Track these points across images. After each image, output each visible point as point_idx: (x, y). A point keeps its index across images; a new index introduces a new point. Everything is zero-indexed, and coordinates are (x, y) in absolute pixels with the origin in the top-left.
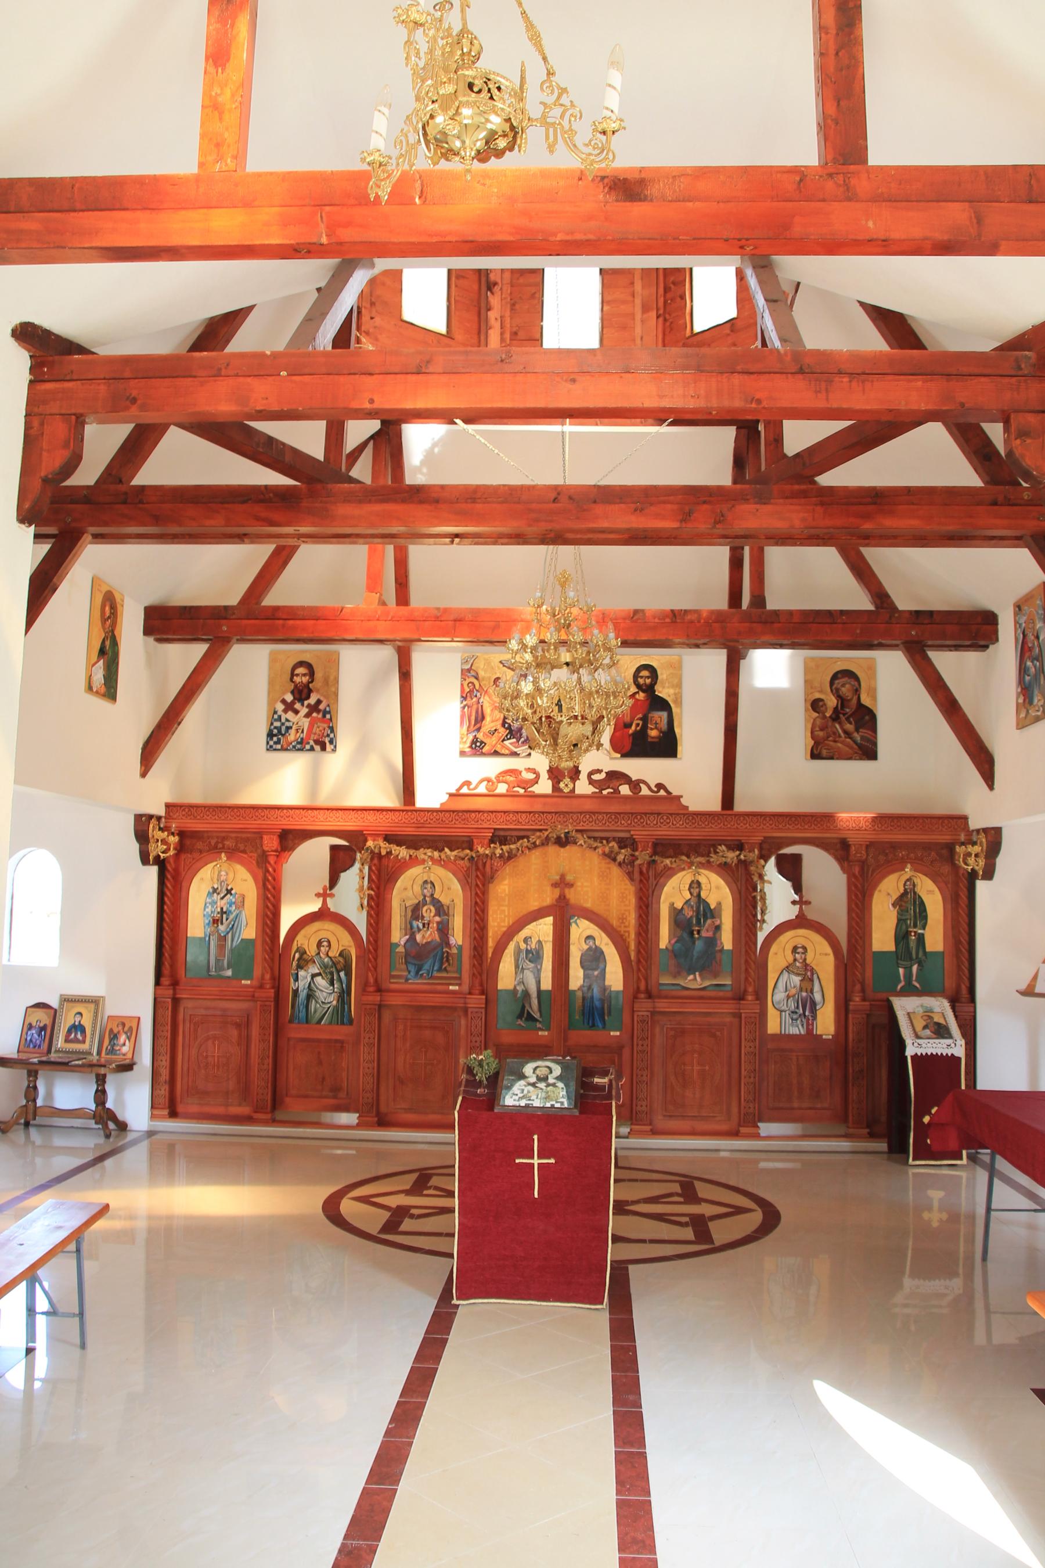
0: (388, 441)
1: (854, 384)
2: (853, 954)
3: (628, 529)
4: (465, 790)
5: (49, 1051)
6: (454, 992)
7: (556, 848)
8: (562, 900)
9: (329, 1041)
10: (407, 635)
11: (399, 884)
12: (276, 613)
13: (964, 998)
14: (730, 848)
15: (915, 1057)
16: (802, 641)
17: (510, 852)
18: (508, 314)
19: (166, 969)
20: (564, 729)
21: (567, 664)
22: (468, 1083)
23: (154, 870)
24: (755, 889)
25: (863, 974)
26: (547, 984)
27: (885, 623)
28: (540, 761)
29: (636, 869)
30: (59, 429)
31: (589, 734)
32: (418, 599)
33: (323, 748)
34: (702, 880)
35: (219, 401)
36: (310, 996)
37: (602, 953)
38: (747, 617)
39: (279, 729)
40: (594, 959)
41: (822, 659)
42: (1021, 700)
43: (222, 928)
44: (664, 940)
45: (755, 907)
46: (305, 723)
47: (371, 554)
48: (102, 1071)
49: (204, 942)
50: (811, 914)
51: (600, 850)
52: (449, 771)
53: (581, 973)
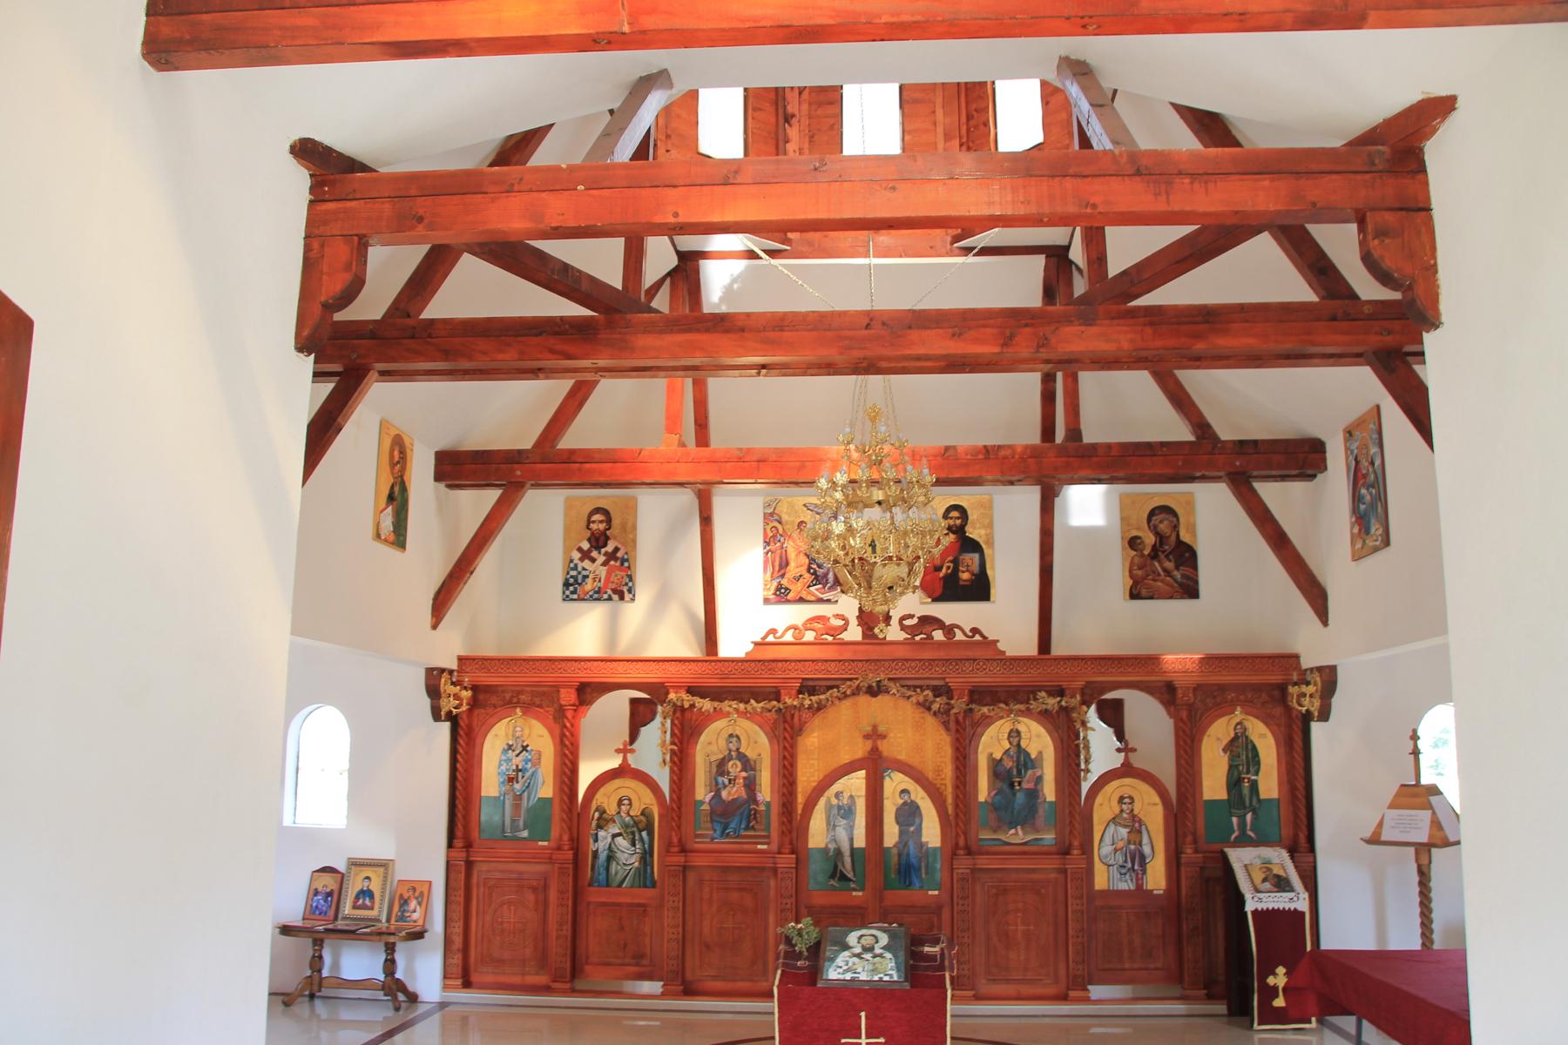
0: (687, 269)
1: (1196, 185)
2: (1181, 802)
3: (945, 357)
4: (771, 639)
5: (336, 918)
6: (762, 852)
7: (868, 698)
8: (875, 751)
9: (631, 905)
10: (708, 478)
11: (703, 738)
12: (571, 456)
13: (1302, 845)
14: (1051, 694)
15: (1255, 912)
16: (1121, 474)
17: (819, 703)
18: (806, 145)
19: (459, 832)
20: (878, 571)
21: (879, 503)
22: (787, 955)
23: (447, 725)
24: (1078, 737)
25: (1194, 823)
26: (860, 842)
27: (1207, 454)
28: (848, 605)
29: (952, 718)
30: (340, 251)
31: (905, 575)
32: (719, 438)
33: (622, 598)
34: (1021, 728)
35: (508, 217)
36: (610, 858)
37: (918, 807)
38: (1062, 450)
39: (575, 578)
40: (909, 814)
41: (1138, 494)
42: (1356, 530)
43: (517, 786)
44: (983, 793)
45: (1078, 756)
46: (603, 572)
47: (671, 390)
48: (392, 939)
49: (498, 801)
50: (1137, 762)
51: (914, 699)
52: (751, 619)
53: (896, 829)
